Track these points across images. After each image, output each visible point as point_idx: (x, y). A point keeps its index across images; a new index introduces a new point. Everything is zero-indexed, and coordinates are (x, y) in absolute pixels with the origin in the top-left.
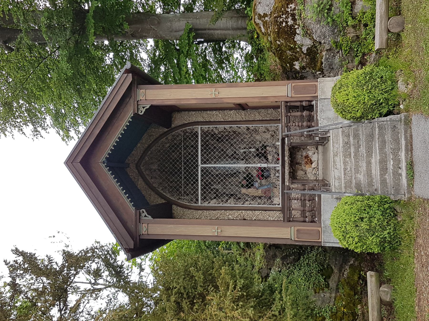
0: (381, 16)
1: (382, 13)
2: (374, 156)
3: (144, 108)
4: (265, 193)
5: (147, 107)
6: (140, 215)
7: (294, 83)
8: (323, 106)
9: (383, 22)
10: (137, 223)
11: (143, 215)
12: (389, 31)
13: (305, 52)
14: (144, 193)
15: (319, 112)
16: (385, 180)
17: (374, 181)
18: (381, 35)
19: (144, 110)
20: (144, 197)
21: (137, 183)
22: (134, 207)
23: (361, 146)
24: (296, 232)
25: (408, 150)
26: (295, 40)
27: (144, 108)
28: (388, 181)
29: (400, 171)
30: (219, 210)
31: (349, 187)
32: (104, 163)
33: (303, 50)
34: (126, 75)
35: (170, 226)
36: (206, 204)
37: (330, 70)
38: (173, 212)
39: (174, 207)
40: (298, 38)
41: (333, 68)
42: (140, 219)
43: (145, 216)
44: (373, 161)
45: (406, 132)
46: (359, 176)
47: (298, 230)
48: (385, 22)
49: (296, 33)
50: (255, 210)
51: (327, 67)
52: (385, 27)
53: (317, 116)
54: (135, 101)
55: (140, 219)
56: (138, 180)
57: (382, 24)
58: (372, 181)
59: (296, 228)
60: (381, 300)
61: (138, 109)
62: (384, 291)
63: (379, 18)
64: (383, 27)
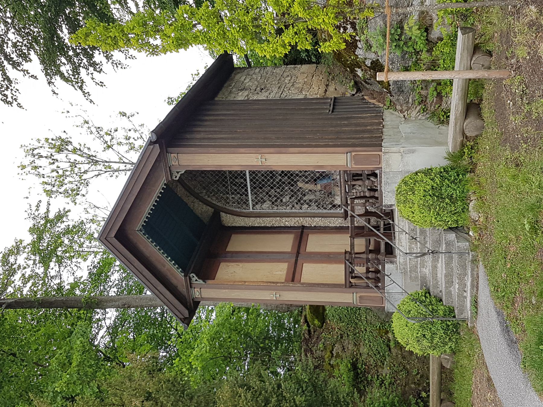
0: (456, 119)
1: (458, 115)
2: (440, 261)
3: (178, 172)
4: (325, 188)
5: (182, 172)
6: (190, 279)
7: (354, 151)
8: (388, 178)
9: (458, 124)
10: (188, 289)
11: (194, 279)
12: (463, 134)
13: (369, 65)
14: (185, 200)
15: (383, 183)
16: (450, 291)
17: (439, 283)
18: (454, 138)
19: (178, 176)
20: (187, 204)
21: (175, 190)
22: (182, 272)
23: (428, 243)
24: (358, 298)
25: (473, 287)
26: (356, 53)
27: (178, 172)
28: (453, 293)
29: (465, 294)
30: (274, 217)
31: (414, 271)
32: (141, 230)
33: (366, 63)
34: (152, 147)
35: (224, 291)
36: (258, 209)
37: (399, 93)
38: (222, 219)
39: (223, 214)
40: (358, 52)
41: (402, 91)
42: (191, 283)
43: (196, 280)
44: (439, 265)
45: (472, 270)
46: (424, 270)
47: (360, 297)
48: (460, 123)
49: (357, 46)
50: (314, 217)
51: (396, 90)
52: (460, 129)
53: (381, 187)
54: (166, 167)
55: (191, 283)
56: (177, 187)
57: (457, 127)
58: (437, 283)
59: (358, 295)
60: (442, 365)
61: (171, 175)
62: (446, 359)
63: (453, 120)
64: (458, 129)
